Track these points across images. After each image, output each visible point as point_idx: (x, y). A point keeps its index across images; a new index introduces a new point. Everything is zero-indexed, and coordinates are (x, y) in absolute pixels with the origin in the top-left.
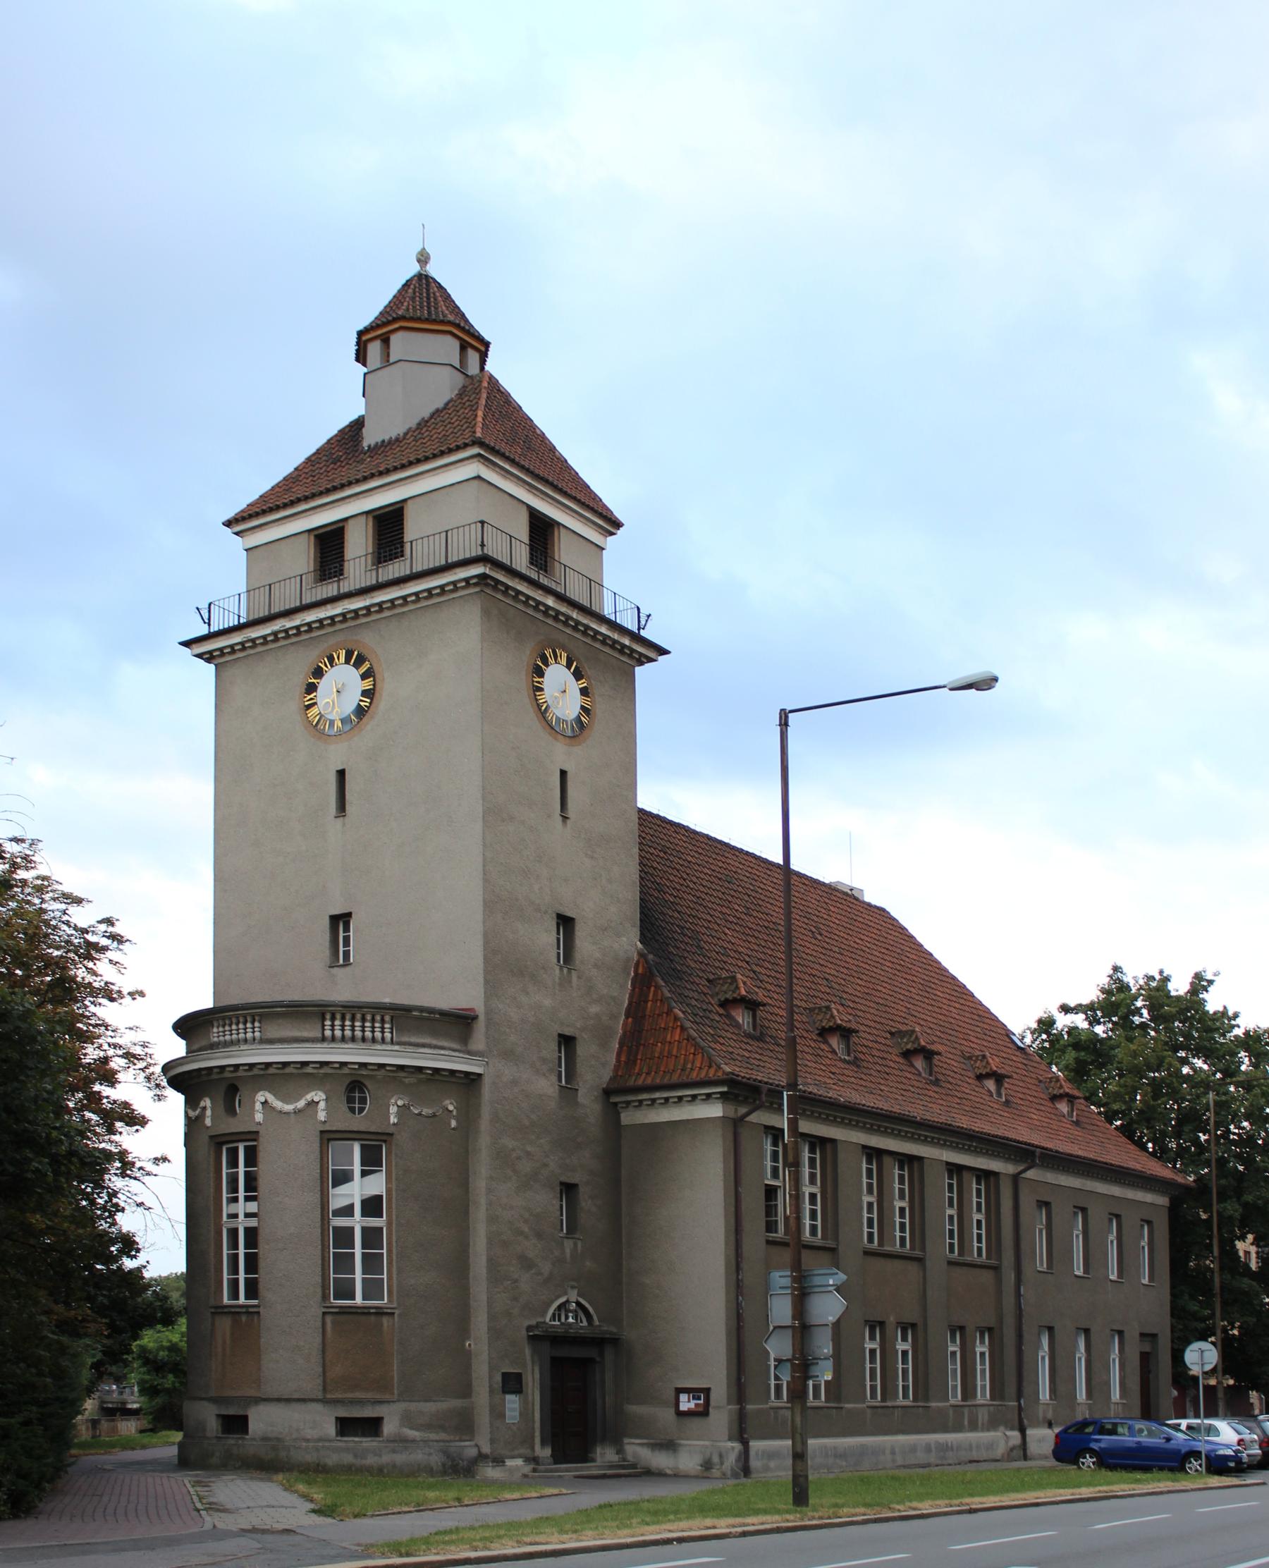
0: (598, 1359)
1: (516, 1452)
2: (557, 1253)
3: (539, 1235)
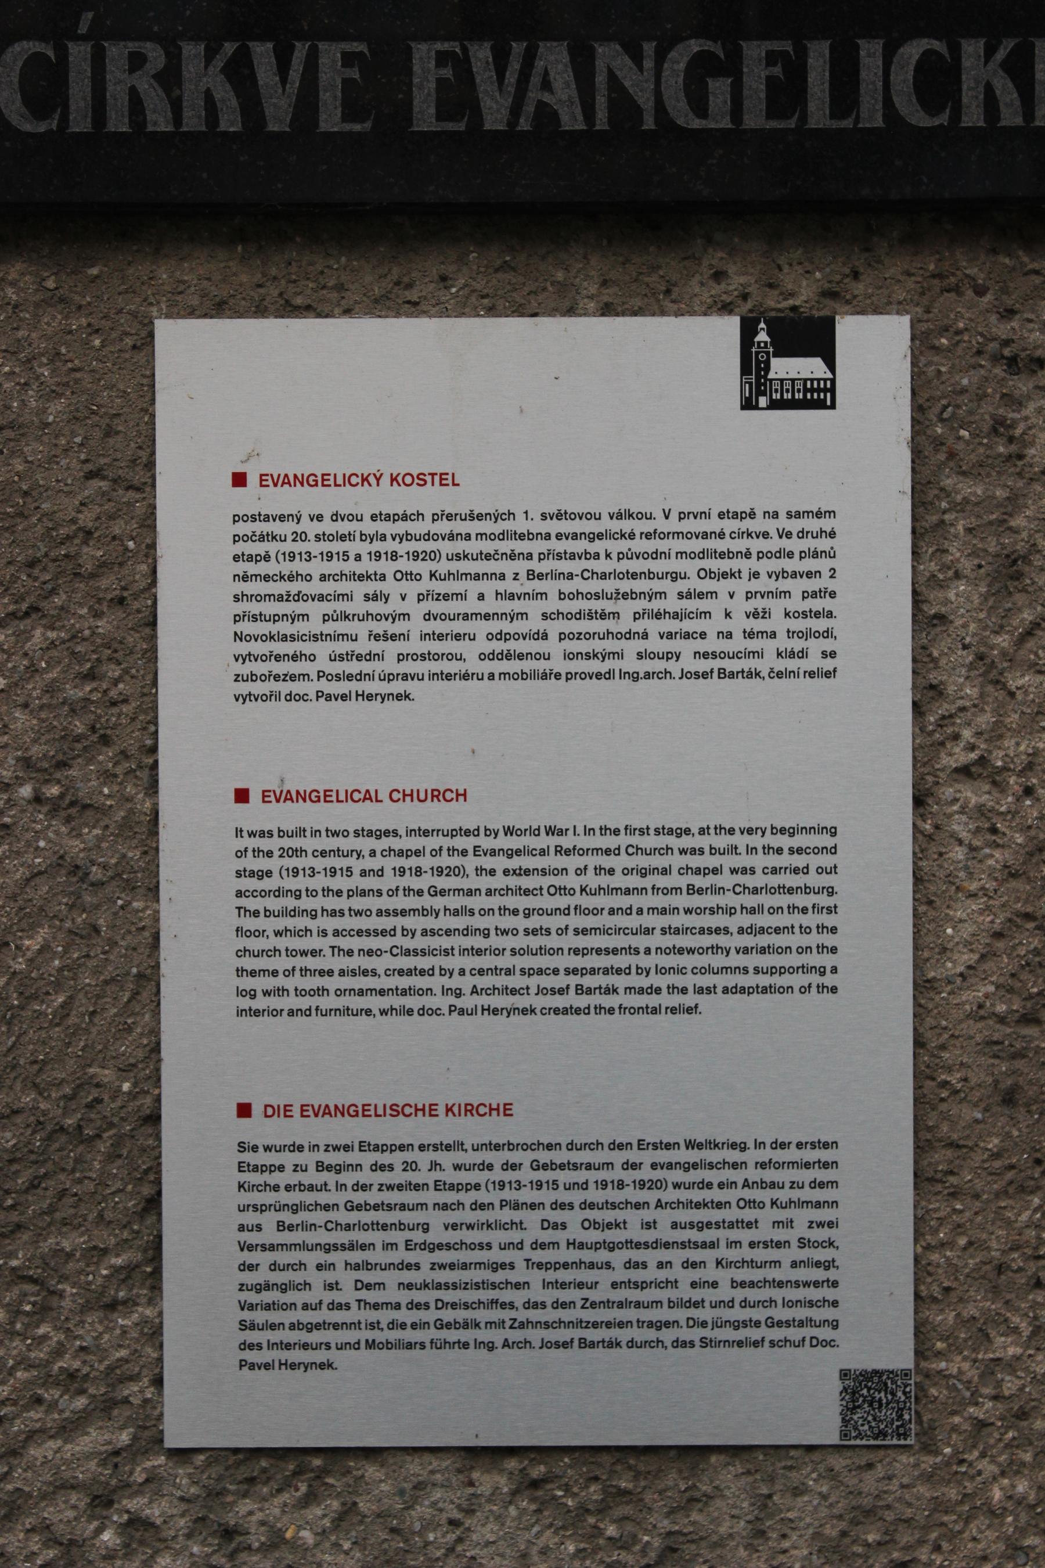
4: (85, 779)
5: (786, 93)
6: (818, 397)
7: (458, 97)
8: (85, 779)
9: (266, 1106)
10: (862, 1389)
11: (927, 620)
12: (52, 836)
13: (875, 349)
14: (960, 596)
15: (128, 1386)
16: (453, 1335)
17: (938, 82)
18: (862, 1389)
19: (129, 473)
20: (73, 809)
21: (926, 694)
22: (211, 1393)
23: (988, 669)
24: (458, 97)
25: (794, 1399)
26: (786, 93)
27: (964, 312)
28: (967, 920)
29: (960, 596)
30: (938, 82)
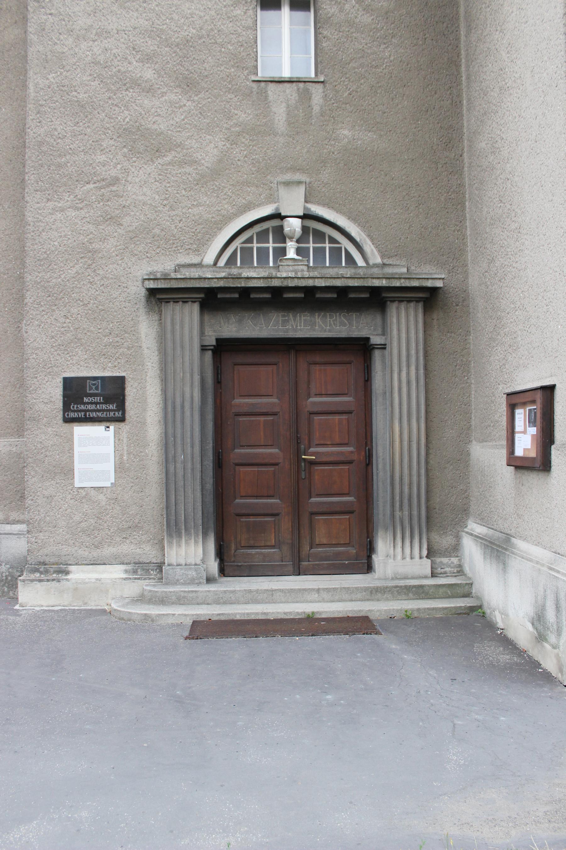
0: (376, 340)
1: (108, 551)
2: (245, 115)
3: (188, 84)
4: (70, 451)
5: (106, 415)
6: (109, 431)
7: (89, 415)
8: (70, 451)
9: (542, 463)
10: (112, 483)
11: (115, 442)
12: (68, 454)
13: (112, 428)
14: (116, 441)
15: (73, 484)
16: (557, 577)
17: (114, 414)
18: (112, 483)
19: (72, 435)
20: (70, 453)
21: (115, 446)
22: (77, 485)
23: (118, 445)
24: (89, 415)
25: (109, 485)
26: (106, 415)
27: (117, 426)
28: (117, 458)
29: (116, 441)
30: (114, 414)
